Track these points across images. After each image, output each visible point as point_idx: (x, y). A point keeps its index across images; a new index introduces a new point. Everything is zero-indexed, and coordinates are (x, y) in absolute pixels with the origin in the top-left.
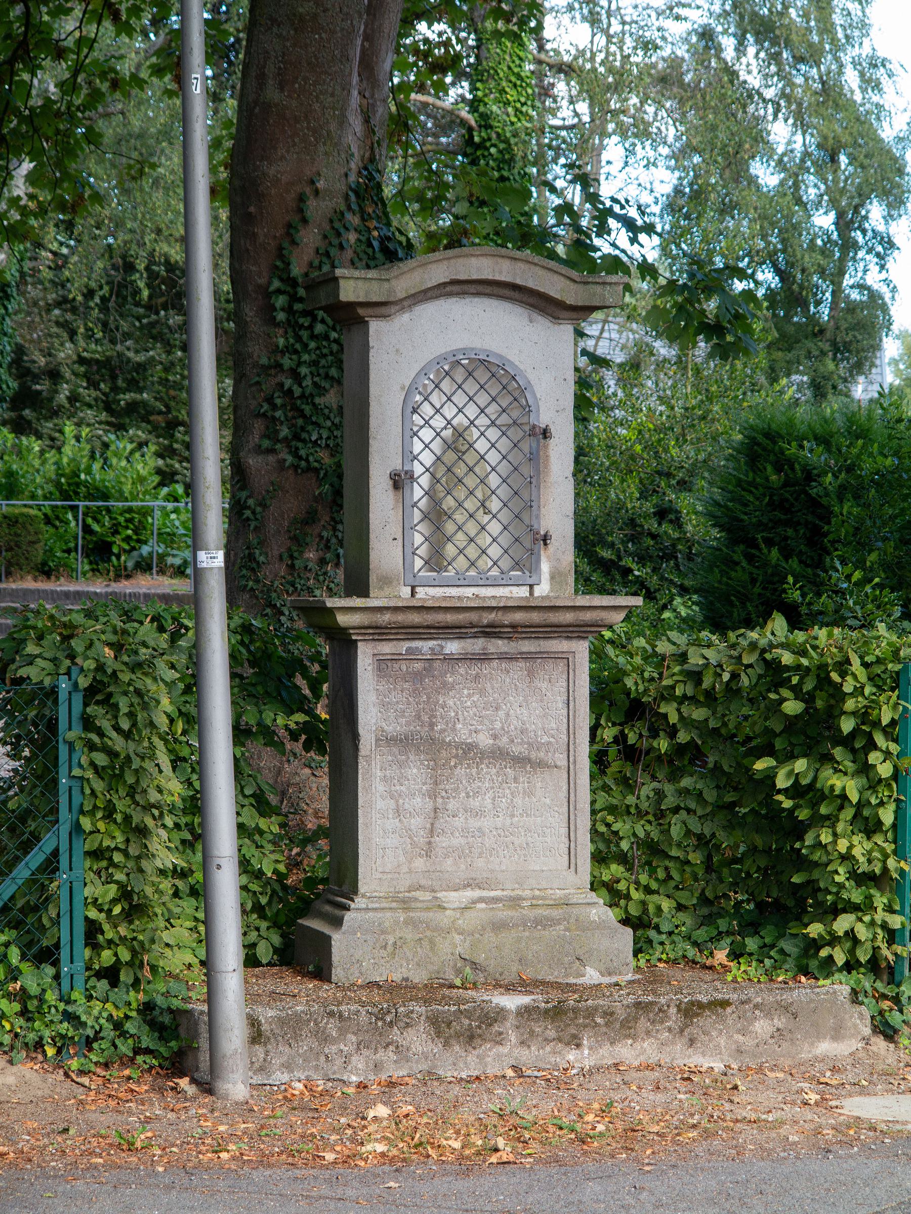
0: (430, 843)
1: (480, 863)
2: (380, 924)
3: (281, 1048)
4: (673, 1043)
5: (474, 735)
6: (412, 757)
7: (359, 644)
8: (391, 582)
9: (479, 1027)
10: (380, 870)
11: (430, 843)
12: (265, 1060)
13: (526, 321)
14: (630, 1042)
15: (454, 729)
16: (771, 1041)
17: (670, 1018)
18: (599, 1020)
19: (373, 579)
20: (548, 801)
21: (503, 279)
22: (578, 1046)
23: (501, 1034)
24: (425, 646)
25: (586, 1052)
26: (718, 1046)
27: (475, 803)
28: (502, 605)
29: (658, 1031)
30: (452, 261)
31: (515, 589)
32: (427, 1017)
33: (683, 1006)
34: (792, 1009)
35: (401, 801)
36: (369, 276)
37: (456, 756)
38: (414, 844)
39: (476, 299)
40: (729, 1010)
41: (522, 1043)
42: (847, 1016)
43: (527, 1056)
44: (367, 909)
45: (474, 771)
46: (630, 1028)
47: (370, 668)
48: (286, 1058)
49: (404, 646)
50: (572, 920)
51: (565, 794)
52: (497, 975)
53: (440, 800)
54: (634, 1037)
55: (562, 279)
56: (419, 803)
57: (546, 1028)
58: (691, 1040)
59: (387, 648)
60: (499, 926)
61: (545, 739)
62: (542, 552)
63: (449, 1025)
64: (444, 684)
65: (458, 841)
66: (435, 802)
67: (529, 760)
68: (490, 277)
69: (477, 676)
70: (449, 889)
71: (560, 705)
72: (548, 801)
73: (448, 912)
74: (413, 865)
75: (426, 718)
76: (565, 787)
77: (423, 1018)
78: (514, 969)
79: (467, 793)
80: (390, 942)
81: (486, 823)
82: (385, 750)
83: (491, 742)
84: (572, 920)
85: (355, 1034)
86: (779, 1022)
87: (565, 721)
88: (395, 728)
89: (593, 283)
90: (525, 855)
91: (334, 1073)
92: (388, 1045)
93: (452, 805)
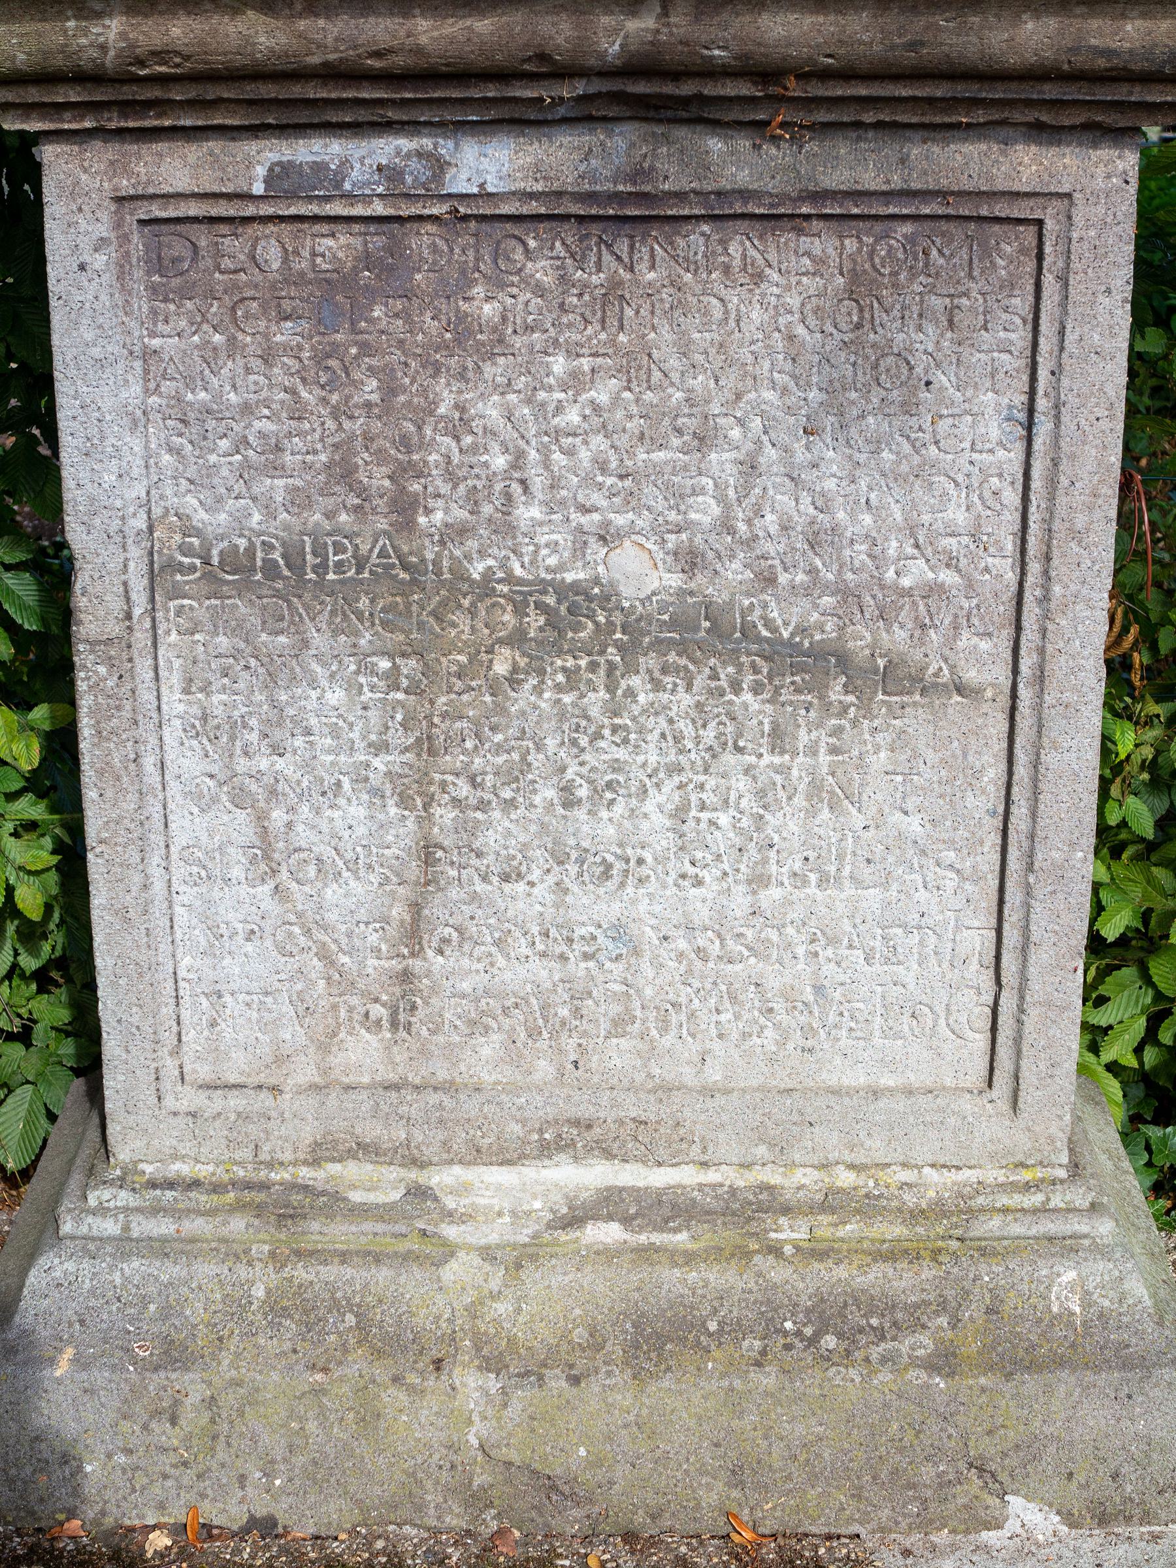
0: (406, 976)
2: (165, 1314)
5: (597, 550)
6: (319, 640)
7: (48, 153)
10: (204, 1072)
11: (406, 976)
15: (505, 527)
20: (914, 825)
35: (278, 816)
37: (517, 639)
44: (125, 1246)
45: (596, 699)
47: (99, 261)
50: (973, 1312)
51: (993, 797)
53: (445, 815)
61: (917, 573)
66: (426, 819)
67: (844, 661)
70: (477, 1155)
71: (993, 430)
72: (914, 825)
74: (337, 1059)
75: (379, 479)
76: (994, 772)
79: (567, 789)
82: (199, 608)
83: (674, 580)
84: (973, 1312)
87: (1012, 497)
88: (239, 521)
90: (808, 1031)
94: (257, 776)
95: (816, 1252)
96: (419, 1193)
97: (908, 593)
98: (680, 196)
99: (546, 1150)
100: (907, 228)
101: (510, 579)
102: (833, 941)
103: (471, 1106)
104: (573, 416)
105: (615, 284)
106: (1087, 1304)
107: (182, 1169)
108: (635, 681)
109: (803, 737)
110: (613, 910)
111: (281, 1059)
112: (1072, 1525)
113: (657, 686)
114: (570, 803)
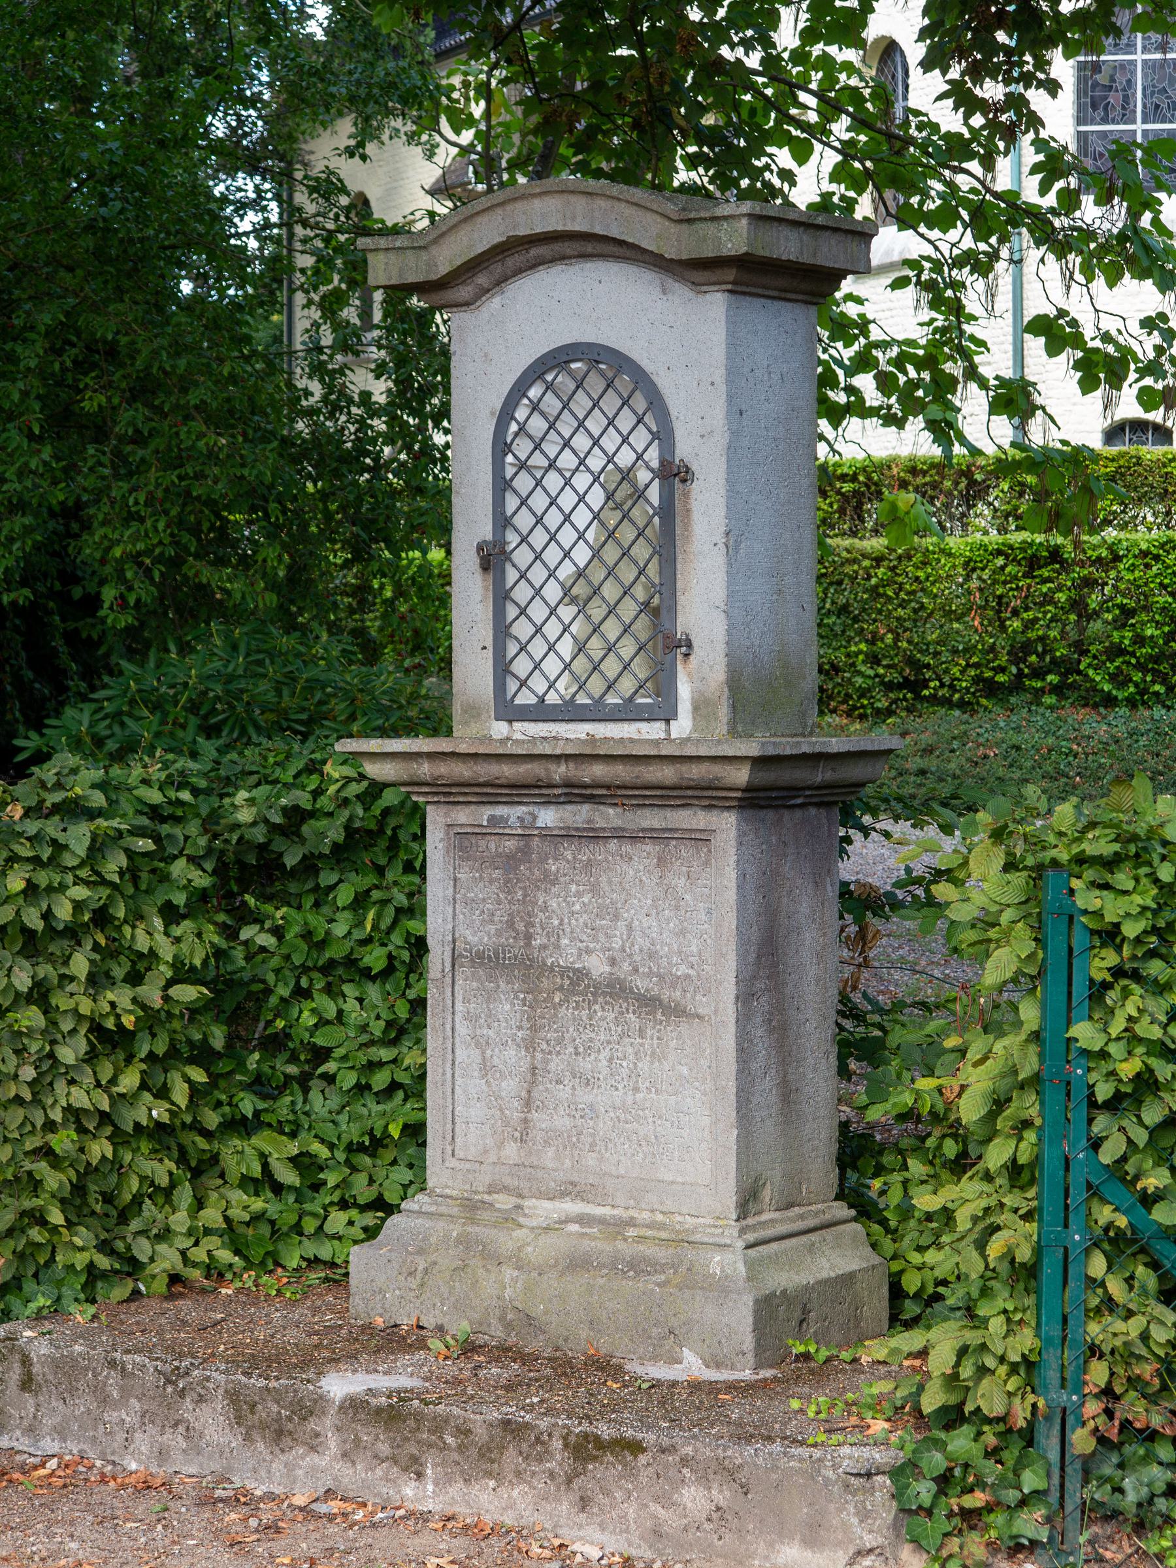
0: (525, 1121)
1: (591, 1160)
3: (54, 1404)
4: (558, 1501)
7: (429, 808)
8: (479, 715)
9: (290, 1419)
11: (525, 1121)
12: (35, 1417)
13: (656, 292)
14: (492, 1483)
15: (557, 947)
16: (708, 1526)
17: (552, 1456)
18: (450, 1440)
19: (457, 710)
20: (685, 1070)
21: (577, 228)
22: (420, 1475)
23: (317, 1435)
24: (513, 813)
25: (430, 1487)
26: (624, 1517)
27: (585, 1065)
28: (558, 751)
29: (534, 1473)
30: (509, 208)
31: (644, 726)
32: (226, 1391)
33: (572, 1439)
34: (742, 1477)
35: (489, 1052)
36: (398, 244)
37: (561, 988)
38: (507, 1124)
39: (589, 265)
40: (643, 1459)
41: (344, 1455)
42: (832, 1507)
43: (352, 1476)
44: (420, 1213)
45: (585, 1013)
46: (493, 1461)
47: (441, 846)
48: (59, 1419)
49: (485, 813)
50: (682, 1270)
52: (561, 1341)
53: (539, 1055)
54: (498, 1477)
55: (659, 219)
56: (512, 1057)
57: (377, 1439)
58: (582, 1498)
59: (462, 816)
60: (577, 1263)
61: (682, 970)
62: (680, 667)
63: (253, 1407)
64: (546, 874)
65: (562, 1122)
66: (533, 1057)
68: (560, 228)
69: (589, 864)
70: (540, 1195)
72: (685, 1070)
73: (518, 1233)
74: (502, 1154)
75: (521, 927)
77: (221, 1391)
78: (584, 1335)
80: (420, 1268)
81: (600, 1097)
83: (608, 969)
85: (140, 1400)
86: (721, 1495)
88: (481, 939)
89: (701, 219)
91: (113, 1453)
92: (176, 1425)
93: (556, 1064)
94: (482, 1036)
95: (641, 1239)
96: (518, 1207)
97: (679, 978)
98: (603, 829)
99: (564, 1194)
100: (674, 842)
101: (559, 966)
102: (660, 1117)
103: (540, 1174)
104: (577, 907)
105: (589, 860)
106: (722, 1271)
107: (448, 1191)
108: (597, 1007)
109: (649, 1032)
110: (589, 1098)
111: (485, 1152)
112: (707, 1366)
113: (603, 1009)
114: (577, 1054)
